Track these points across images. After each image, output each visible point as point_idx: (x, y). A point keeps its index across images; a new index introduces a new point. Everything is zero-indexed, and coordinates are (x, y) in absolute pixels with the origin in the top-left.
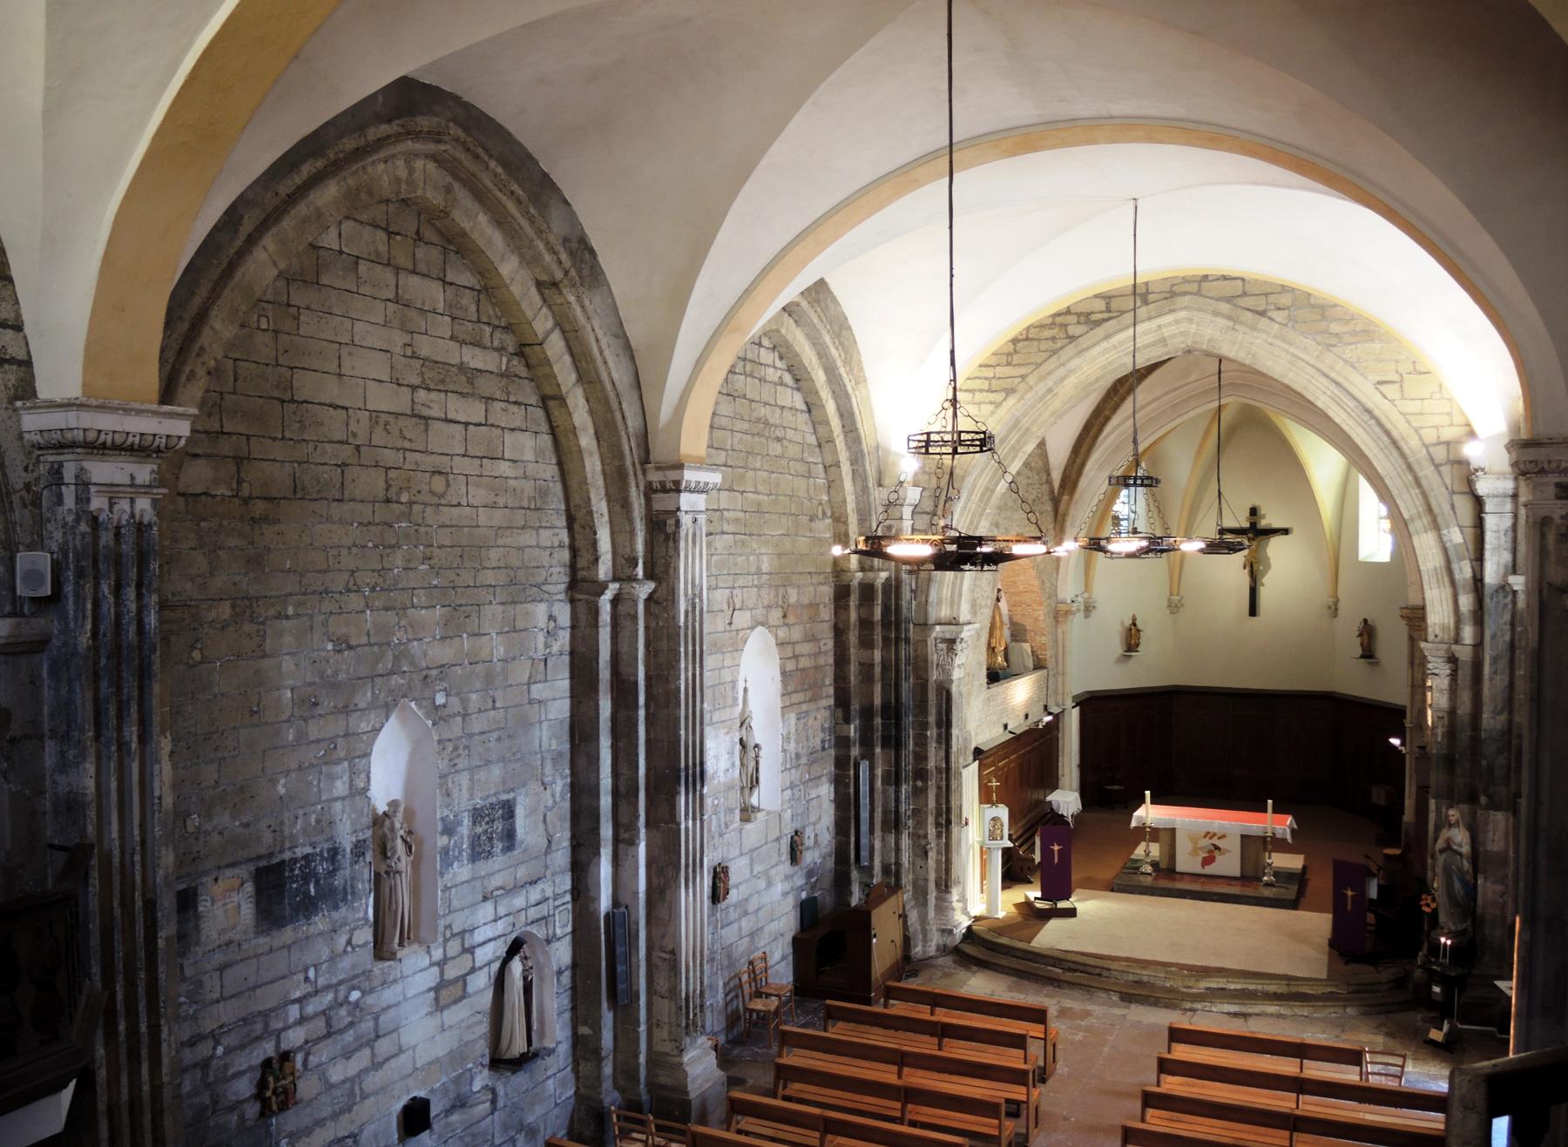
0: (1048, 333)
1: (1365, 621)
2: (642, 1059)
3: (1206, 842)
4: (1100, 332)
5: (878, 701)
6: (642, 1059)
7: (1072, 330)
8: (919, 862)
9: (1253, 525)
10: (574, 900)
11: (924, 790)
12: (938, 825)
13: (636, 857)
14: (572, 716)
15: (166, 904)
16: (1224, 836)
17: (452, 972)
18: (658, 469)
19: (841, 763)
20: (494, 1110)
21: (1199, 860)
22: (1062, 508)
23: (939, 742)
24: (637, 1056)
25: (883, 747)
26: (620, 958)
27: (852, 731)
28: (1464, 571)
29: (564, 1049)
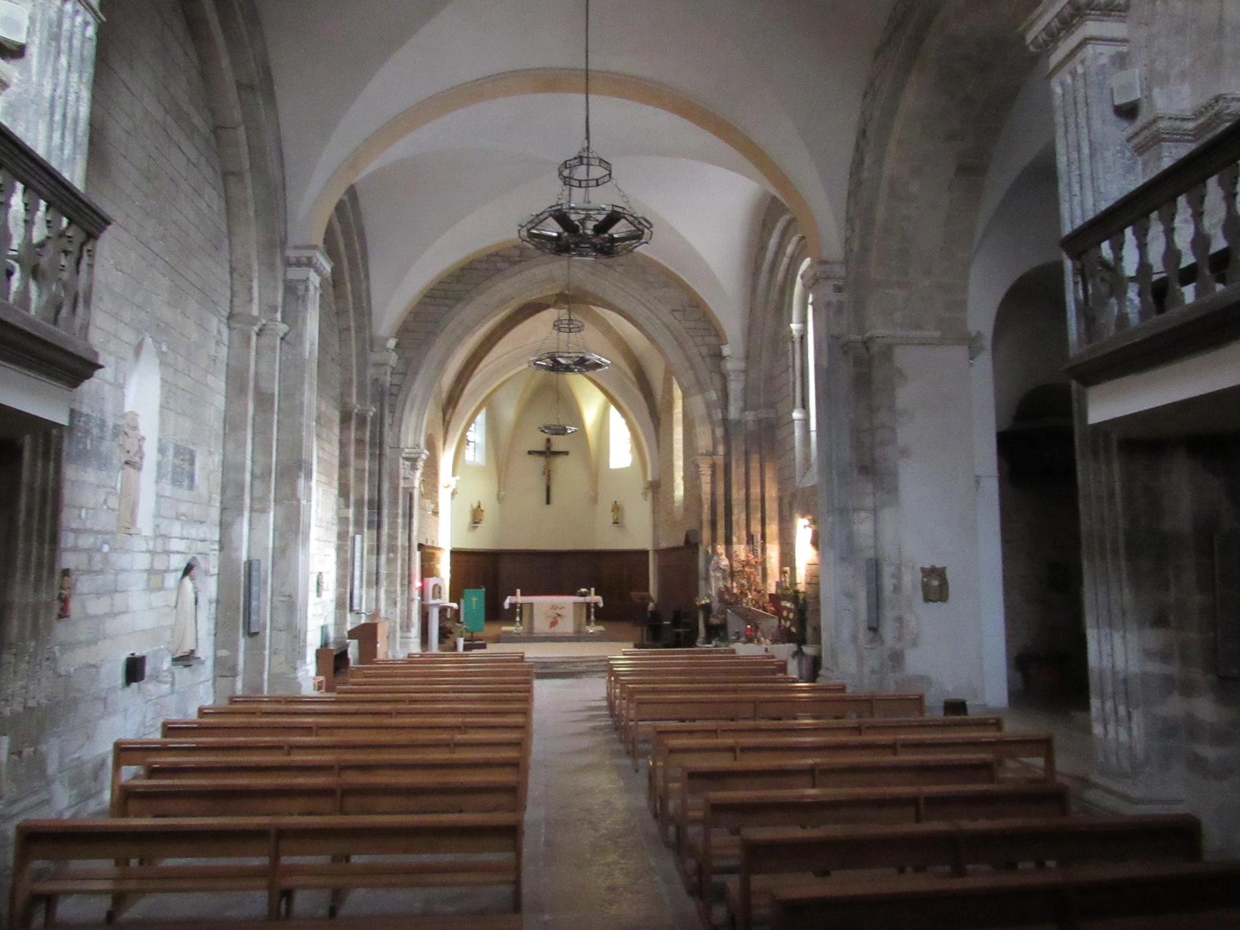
0: (484, 266)
2: (266, 676)
3: (552, 613)
4: (517, 268)
5: (366, 497)
6: (266, 676)
7: (500, 265)
8: (391, 610)
9: (548, 448)
10: (221, 549)
11: (395, 559)
12: (402, 585)
13: (267, 521)
14: (226, 411)
17: (159, 565)
18: (296, 248)
19: (342, 536)
20: (172, 693)
23: (404, 528)
24: (262, 673)
25: (369, 528)
26: (254, 595)
27: (351, 513)
28: (718, 415)
29: (209, 663)
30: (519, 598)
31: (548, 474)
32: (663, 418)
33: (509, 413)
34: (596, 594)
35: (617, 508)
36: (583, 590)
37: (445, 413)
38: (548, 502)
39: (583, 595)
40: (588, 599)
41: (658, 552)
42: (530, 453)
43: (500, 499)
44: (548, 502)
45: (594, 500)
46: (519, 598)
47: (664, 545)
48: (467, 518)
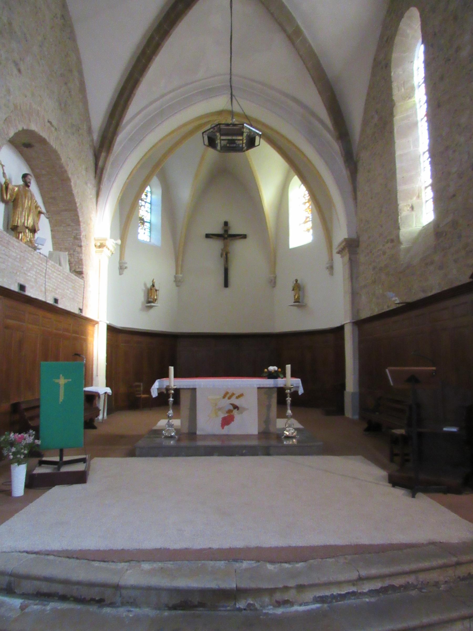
1: (296, 281)
3: (226, 404)
9: (226, 231)
15: (469, 558)
16: (242, 395)
21: (219, 421)
22: (100, 164)
30: (172, 382)
31: (226, 256)
32: (364, 157)
33: (185, 193)
34: (294, 375)
35: (298, 287)
36: (272, 368)
37: (97, 157)
38: (226, 284)
39: (272, 376)
40: (280, 382)
41: (359, 324)
42: (208, 236)
43: (178, 282)
44: (226, 284)
45: (273, 282)
46: (172, 382)
47: (365, 314)
48: (141, 297)
